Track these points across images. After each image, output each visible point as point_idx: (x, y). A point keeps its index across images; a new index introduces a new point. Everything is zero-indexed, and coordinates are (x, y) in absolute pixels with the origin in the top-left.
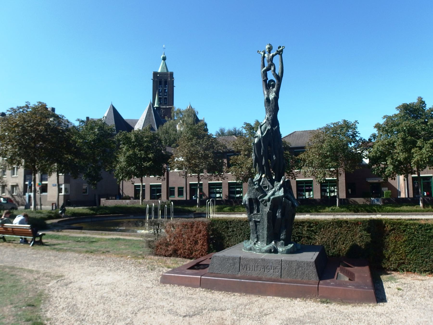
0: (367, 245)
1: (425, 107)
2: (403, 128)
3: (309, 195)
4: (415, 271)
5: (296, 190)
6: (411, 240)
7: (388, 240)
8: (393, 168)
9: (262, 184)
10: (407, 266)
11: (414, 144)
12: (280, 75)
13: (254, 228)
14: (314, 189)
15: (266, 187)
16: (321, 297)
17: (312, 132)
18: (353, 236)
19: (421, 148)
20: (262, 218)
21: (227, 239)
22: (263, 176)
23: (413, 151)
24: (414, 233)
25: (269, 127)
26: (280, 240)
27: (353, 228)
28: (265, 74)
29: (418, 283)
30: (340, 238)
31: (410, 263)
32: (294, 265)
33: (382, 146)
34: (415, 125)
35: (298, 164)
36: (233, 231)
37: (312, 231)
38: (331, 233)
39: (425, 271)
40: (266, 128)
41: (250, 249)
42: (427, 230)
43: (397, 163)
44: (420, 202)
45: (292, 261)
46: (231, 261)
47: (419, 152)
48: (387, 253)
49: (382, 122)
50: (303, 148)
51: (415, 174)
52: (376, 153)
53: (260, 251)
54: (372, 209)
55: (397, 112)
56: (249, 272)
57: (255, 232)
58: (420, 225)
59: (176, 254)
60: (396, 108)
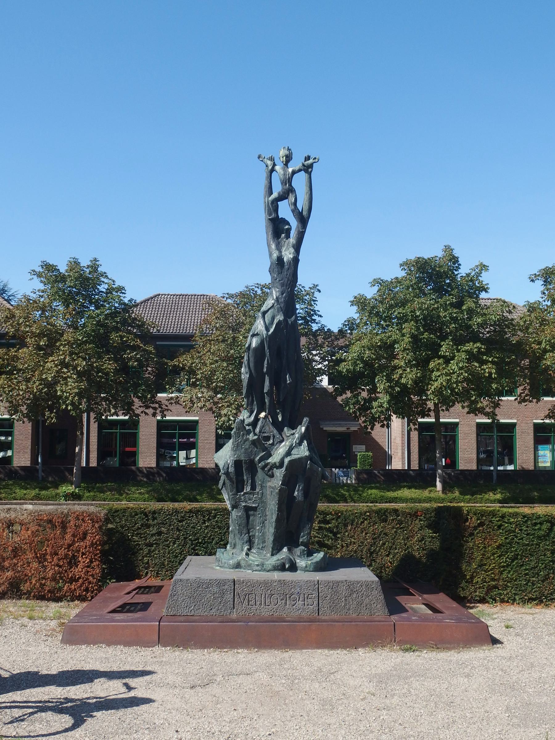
0: (432, 554)
1: (458, 268)
2: (413, 311)
3: (188, 458)
4: (514, 600)
5: (155, 445)
6: (510, 543)
7: (471, 544)
8: (389, 402)
9: (260, 432)
10: (501, 592)
11: (434, 349)
12: (305, 213)
13: (244, 521)
14: (200, 445)
15: (267, 438)
16: (400, 643)
17: (210, 302)
18: (408, 538)
19: (447, 361)
20: (262, 501)
21: (146, 551)
22: (263, 415)
23: (432, 365)
24: (514, 532)
25: (280, 317)
26: (297, 546)
27: (407, 523)
28: (273, 207)
29: (530, 617)
30: (384, 544)
31: (506, 585)
32: (343, 589)
33: (369, 349)
34: (438, 308)
35: (165, 378)
36: (160, 533)
37: (330, 530)
38: (366, 534)
39: (531, 600)
40: (273, 318)
41: (238, 566)
42: (536, 524)
43: (397, 389)
44: (438, 480)
45: (338, 582)
46: (216, 589)
47: (444, 369)
48: (468, 569)
49: (371, 293)
50: (189, 337)
51: (428, 416)
52: (355, 364)
53: (262, 567)
54: (337, 495)
55: (401, 274)
56: (254, 607)
57: (245, 531)
58: (524, 517)
59: (18, 590)
60: (401, 265)
